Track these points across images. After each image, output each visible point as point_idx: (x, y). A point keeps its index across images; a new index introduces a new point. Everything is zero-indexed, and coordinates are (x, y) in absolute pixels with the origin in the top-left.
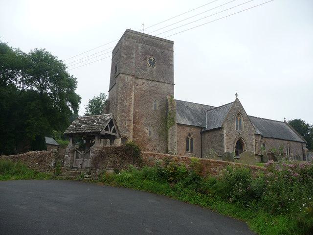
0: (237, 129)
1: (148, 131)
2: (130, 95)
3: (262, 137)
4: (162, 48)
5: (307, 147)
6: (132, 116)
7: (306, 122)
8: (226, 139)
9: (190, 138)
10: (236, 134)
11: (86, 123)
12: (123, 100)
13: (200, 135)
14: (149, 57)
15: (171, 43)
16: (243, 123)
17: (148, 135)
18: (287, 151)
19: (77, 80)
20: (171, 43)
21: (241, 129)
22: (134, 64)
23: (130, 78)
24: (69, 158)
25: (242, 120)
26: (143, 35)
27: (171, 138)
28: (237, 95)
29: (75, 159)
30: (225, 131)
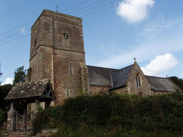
0: (138, 86)
1: (66, 93)
2: (49, 63)
3: (154, 91)
6: (53, 81)
11: (24, 88)
12: (44, 68)
14: (63, 31)
15: (80, 20)
16: (141, 80)
17: (67, 95)
20: (80, 20)
21: (140, 86)
22: (52, 38)
23: (49, 48)
24: (12, 122)
25: (141, 78)
26: (57, 13)
28: (135, 59)
29: (17, 121)
30: (129, 88)
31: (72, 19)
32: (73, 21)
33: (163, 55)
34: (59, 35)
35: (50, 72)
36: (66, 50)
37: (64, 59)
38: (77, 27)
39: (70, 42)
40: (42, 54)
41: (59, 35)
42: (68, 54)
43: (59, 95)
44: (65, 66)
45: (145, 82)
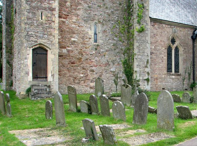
13: (191, 42)
17: (92, 40)
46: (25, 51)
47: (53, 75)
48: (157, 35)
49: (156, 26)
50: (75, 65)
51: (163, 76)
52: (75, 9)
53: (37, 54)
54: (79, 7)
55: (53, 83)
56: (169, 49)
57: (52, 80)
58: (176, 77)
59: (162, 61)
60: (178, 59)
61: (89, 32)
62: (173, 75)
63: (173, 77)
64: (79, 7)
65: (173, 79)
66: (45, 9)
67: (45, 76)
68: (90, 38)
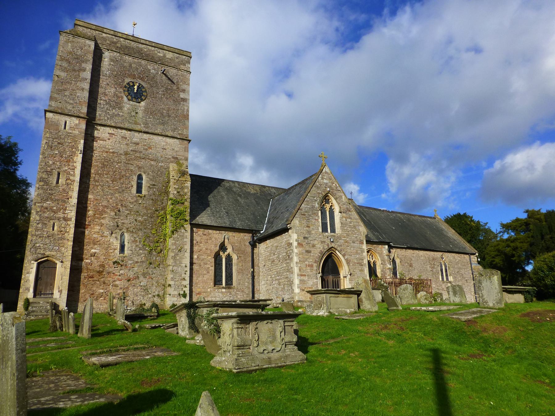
0: (325, 229)
4: (161, 62)
5: (479, 263)
7: (476, 219)
8: (298, 254)
9: (223, 256)
10: (323, 242)
13: (249, 249)
17: (117, 251)
18: (442, 273)
19: (20, 146)
21: (333, 230)
27: (174, 258)
31: (161, 51)
32: (164, 56)
33: (465, 214)
34: (113, 90)
35: (68, 184)
36: (130, 130)
37: (122, 152)
38: (172, 72)
39: (147, 110)
40: (48, 135)
41: (113, 90)
42: (135, 140)
43: (93, 251)
44: (123, 173)
45: (349, 220)
46: (28, 265)
47: (60, 292)
48: (201, 243)
49: (199, 232)
50: (93, 279)
51: (209, 290)
52: (98, 218)
53: (45, 267)
54: (104, 216)
55: (60, 300)
56: (217, 257)
57: (58, 297)
58: (227, 290)
59: (208, 272)
60: (231, 269)
61: (114, 242)
62: (223, 288)
63: (224, 290)
64: (104, 216)
65: (222, 292)
66: (59, 219)
67: (51, 293)
68: (115, 249)
